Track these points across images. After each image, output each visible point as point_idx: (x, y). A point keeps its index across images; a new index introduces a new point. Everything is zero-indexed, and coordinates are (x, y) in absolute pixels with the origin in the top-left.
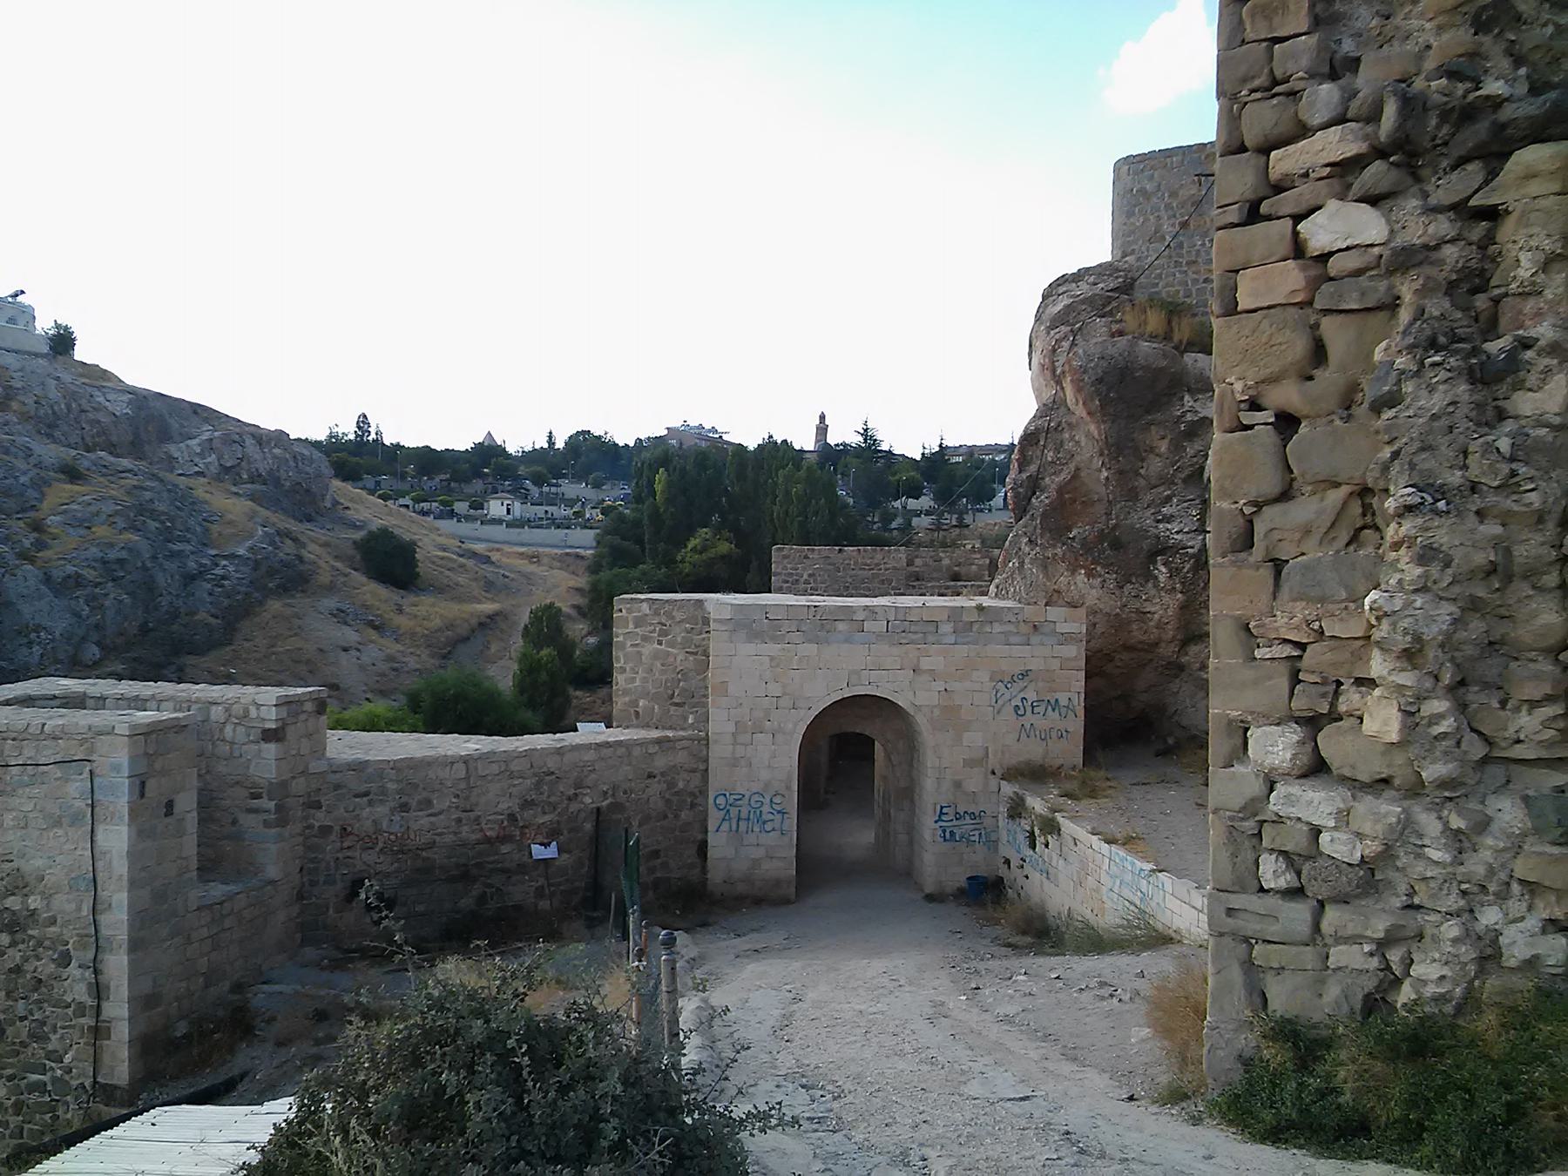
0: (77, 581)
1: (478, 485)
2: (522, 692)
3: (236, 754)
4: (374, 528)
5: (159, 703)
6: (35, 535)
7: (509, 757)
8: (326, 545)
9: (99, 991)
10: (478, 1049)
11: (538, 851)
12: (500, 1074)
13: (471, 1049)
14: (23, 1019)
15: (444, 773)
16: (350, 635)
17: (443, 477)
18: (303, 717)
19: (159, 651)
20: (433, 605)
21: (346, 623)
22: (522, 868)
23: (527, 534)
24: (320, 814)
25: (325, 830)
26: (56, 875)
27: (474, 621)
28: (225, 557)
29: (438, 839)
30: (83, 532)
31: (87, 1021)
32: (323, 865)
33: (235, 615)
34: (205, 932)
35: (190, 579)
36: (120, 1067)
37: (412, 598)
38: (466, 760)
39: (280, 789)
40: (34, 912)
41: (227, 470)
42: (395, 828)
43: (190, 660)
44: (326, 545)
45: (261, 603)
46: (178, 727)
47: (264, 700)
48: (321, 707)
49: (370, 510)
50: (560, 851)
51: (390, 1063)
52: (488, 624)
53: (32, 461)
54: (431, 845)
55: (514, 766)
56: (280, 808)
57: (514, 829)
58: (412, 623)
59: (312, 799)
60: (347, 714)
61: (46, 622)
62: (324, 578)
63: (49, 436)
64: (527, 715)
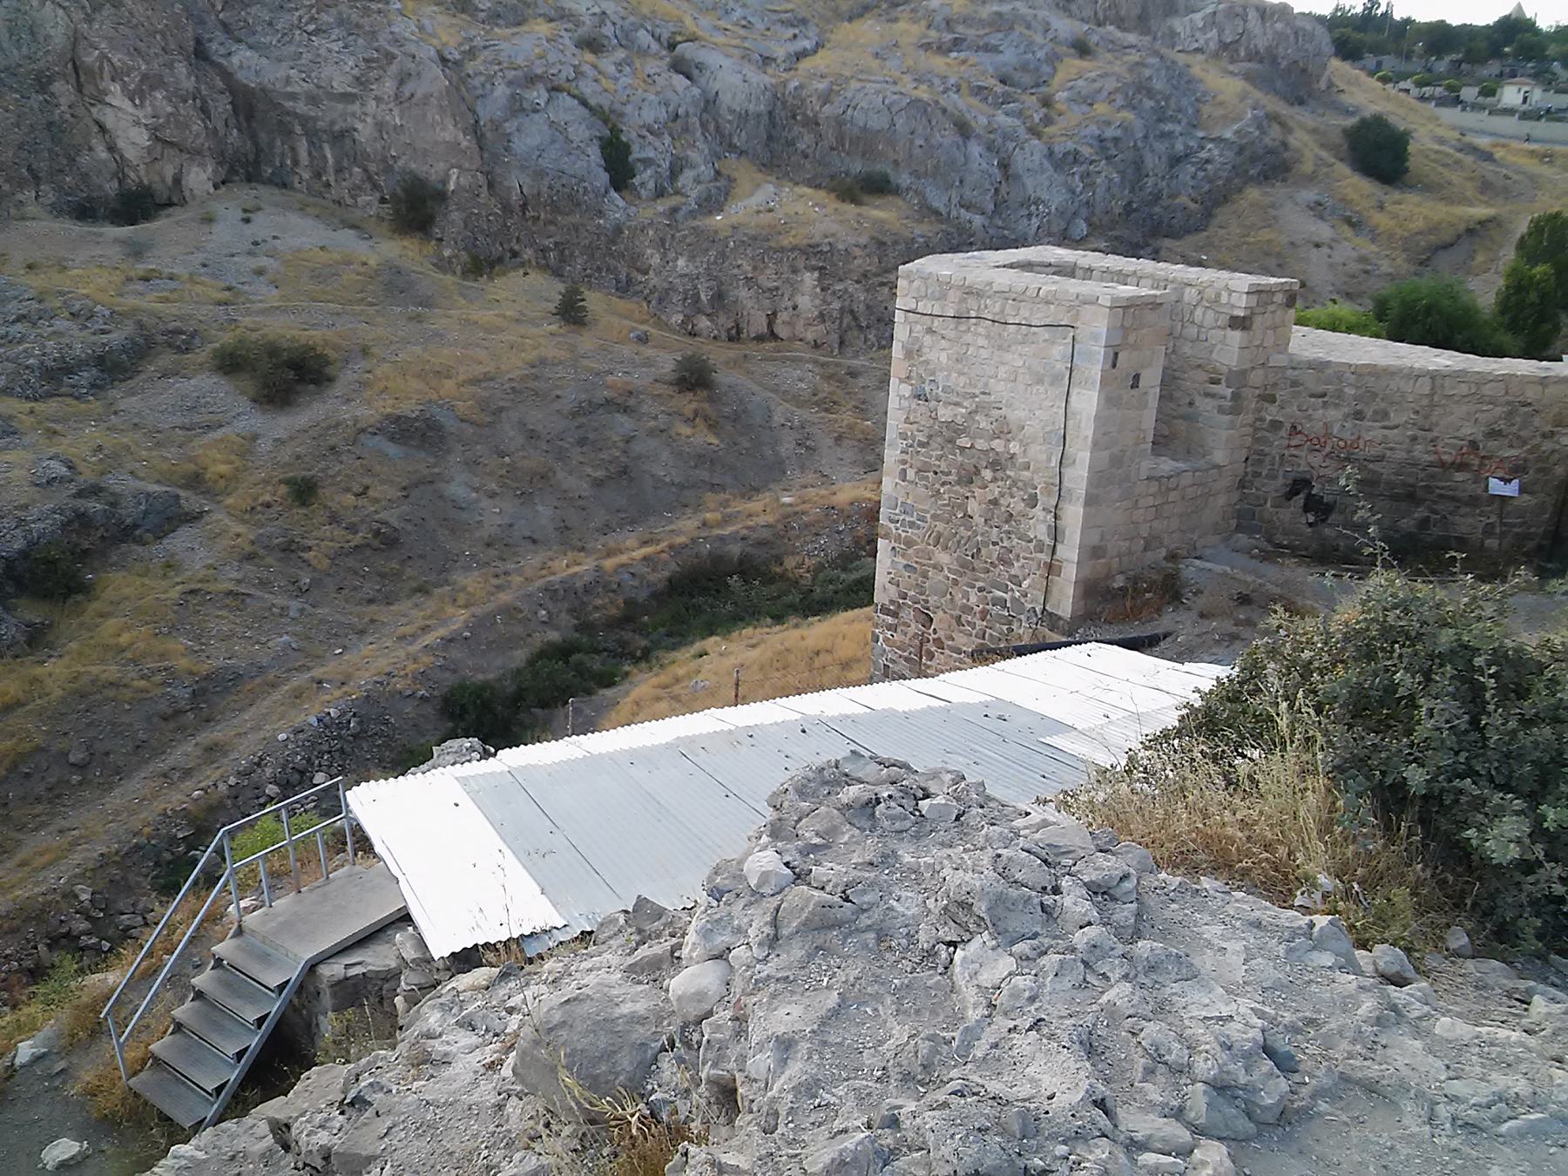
0: (1075, 157)
1: (1493, 68)
2: (1503, 313)
3: (1203, 337)
4: (1367, 114)
5: (1138, 278)
6: (1044, 110)
7: (1483, 379)
8: (1314, 131)
9: (1056, 534)
10: (1443, 658)
11: (1496, 486)
12: (1457, 689)
13: (1431, 657)
14: (995, 544)
15: (1407, 387)
16: (1324, 231)
17: (1454, 57)
18: (1271, 308)
19: (1141, 228)
20: (1419, 205)
21: (1322, 218)
22: (1474, 501)
23: (1542, 128)
24: (1273, 409)
25: (1276, 425)
26: (1033, 427)
27: (1462, 227)
28: (1212, 140)
29: (1388, 453)
30: (1085, 108)
31: (1044, 557)
32: (1268, 459)
33: (1216, 199)
34: (1150, 501)
35: (1176, 161)
36: (1065, 603)
37: (1397, 195)
38: (1434, 376)
39: (1239, 378)
40: (1013, 456)
41: (1224, 46)
42: (1347, 435)
43: (1167, 242)
44: (1314, 131)
45: (1240, 191)
46: (1154, 305)
47: (1237, 286)
48: (1291, 301)
49: (1364, 93)
50: (1522, 490)
51: (1344, 649)
52: (1475, 231)
53: (1050, 35)
54: (1380, 459)
55: (1487, 390)
56: (1236, 396)
57: (1472, 459)
58: (1392, 223)
59: (1266, 391)
60: (1310, 313)
61: (1045, 196)
62: (1308, 167)
63: (1065, 9)
64: (1506, 339)
